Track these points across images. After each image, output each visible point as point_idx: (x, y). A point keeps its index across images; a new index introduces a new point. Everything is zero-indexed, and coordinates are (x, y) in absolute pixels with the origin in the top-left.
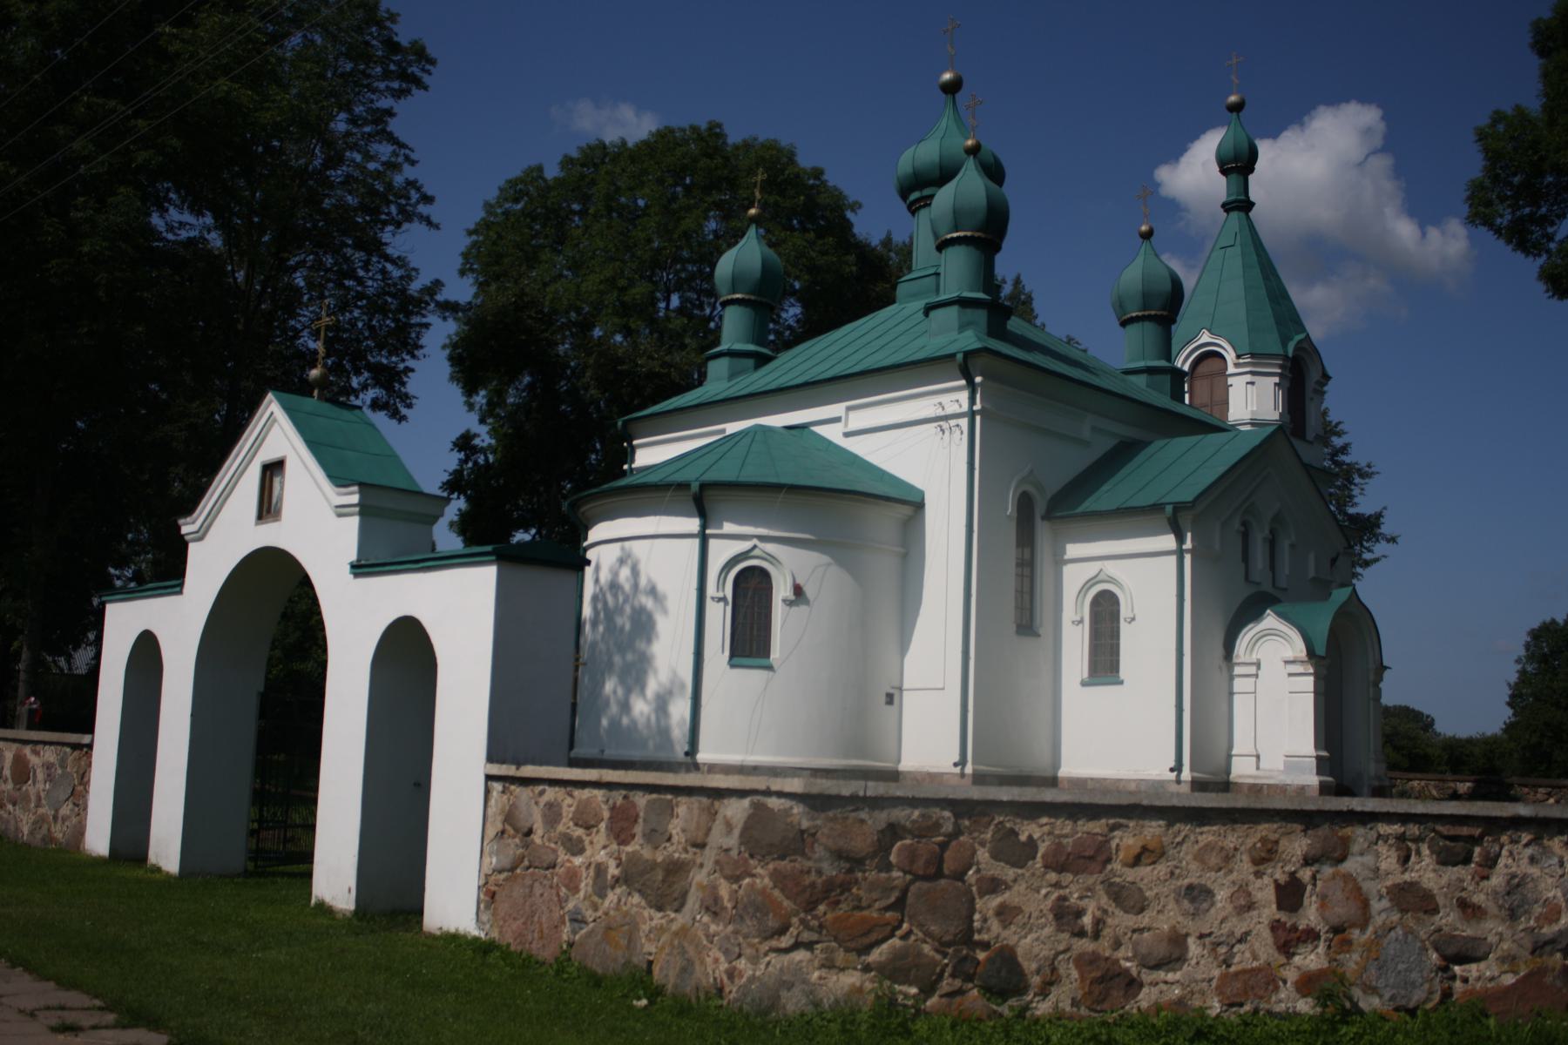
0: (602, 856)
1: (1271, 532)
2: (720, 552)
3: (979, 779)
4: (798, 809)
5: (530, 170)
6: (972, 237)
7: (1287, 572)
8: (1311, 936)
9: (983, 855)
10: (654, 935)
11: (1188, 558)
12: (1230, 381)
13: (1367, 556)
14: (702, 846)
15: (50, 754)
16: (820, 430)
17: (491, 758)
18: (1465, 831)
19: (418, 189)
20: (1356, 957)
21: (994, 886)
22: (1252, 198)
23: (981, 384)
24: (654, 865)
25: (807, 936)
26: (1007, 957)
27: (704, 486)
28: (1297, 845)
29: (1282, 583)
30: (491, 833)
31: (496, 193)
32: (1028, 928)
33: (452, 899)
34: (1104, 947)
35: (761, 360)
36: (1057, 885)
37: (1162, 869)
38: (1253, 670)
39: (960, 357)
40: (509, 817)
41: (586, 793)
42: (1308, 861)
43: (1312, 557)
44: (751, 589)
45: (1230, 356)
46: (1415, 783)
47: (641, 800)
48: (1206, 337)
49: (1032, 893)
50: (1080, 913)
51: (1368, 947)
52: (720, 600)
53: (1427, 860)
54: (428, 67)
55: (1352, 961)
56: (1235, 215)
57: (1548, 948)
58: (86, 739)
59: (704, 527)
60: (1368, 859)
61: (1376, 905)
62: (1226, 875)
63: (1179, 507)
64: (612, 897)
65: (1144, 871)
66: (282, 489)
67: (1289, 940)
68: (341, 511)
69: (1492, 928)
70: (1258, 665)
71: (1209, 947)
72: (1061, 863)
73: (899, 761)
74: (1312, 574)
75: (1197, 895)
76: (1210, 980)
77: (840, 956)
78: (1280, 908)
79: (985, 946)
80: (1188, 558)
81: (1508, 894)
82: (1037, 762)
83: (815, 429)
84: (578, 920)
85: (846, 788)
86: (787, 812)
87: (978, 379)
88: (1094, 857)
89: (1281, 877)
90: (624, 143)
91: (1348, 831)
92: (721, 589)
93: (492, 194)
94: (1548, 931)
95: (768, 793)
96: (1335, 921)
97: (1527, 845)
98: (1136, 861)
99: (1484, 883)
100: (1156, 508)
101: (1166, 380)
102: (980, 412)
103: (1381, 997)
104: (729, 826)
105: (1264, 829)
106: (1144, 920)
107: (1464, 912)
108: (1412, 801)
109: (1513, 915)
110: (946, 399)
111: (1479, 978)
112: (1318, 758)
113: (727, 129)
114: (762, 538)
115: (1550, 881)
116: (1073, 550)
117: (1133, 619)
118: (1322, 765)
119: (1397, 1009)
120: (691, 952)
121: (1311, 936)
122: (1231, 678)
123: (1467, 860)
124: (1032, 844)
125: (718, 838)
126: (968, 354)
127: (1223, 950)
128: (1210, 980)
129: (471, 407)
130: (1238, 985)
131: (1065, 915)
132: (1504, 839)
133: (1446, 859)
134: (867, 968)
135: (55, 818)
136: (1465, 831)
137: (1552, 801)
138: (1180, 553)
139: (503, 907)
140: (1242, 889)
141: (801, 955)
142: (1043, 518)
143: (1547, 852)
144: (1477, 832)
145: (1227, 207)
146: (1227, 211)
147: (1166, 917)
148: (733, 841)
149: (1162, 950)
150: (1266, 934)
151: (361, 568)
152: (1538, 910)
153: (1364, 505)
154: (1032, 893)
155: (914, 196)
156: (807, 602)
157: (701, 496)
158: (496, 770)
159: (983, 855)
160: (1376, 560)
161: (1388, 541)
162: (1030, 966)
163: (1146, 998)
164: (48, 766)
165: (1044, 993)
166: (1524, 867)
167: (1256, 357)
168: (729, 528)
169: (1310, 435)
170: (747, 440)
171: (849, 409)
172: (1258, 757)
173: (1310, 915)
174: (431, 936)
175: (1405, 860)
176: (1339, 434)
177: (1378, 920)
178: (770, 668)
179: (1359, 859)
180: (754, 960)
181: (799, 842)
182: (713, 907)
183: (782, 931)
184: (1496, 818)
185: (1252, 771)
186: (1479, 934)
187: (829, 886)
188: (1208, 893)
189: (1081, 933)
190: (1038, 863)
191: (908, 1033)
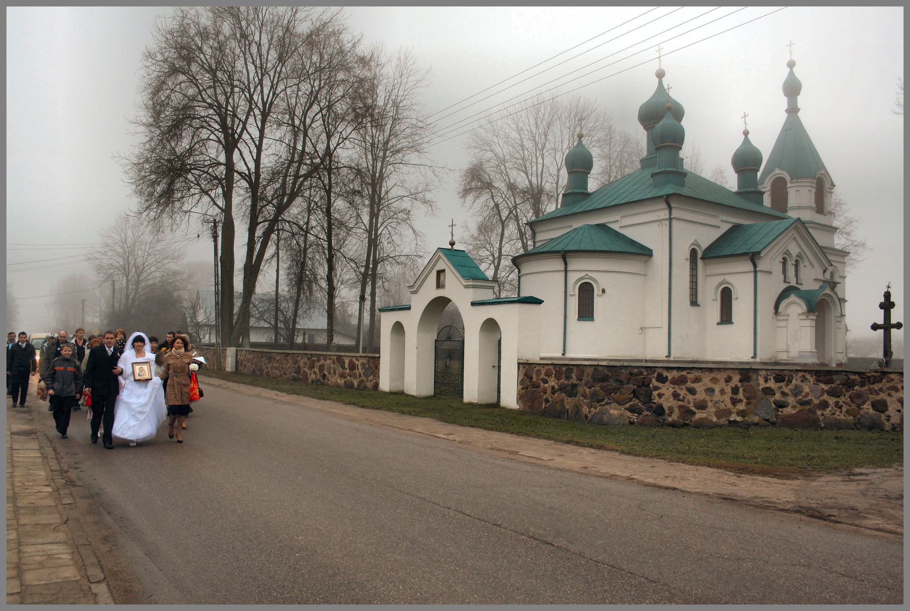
8: (741, 401)
9: (654, 380)
21: (656, 388)
24: (567, 385)
48: (777, 171)
49: (667, 390)
64: (556, 394)
67: (734, 402)
72: (675, 382)
75: (710, 391)
88: (682, 381)
92: (574, 291)
105: (729, 373)
109: (796, 396)
121: (741, 401)
123: (783, 381)
131: (676, 396)
147: (701, 395)
165: (670, 415)
170: (582, 232)
173: (741, 396)
174: (504, 408)
182: (584, 396)
187: (615, 389)
189: (679, 400)
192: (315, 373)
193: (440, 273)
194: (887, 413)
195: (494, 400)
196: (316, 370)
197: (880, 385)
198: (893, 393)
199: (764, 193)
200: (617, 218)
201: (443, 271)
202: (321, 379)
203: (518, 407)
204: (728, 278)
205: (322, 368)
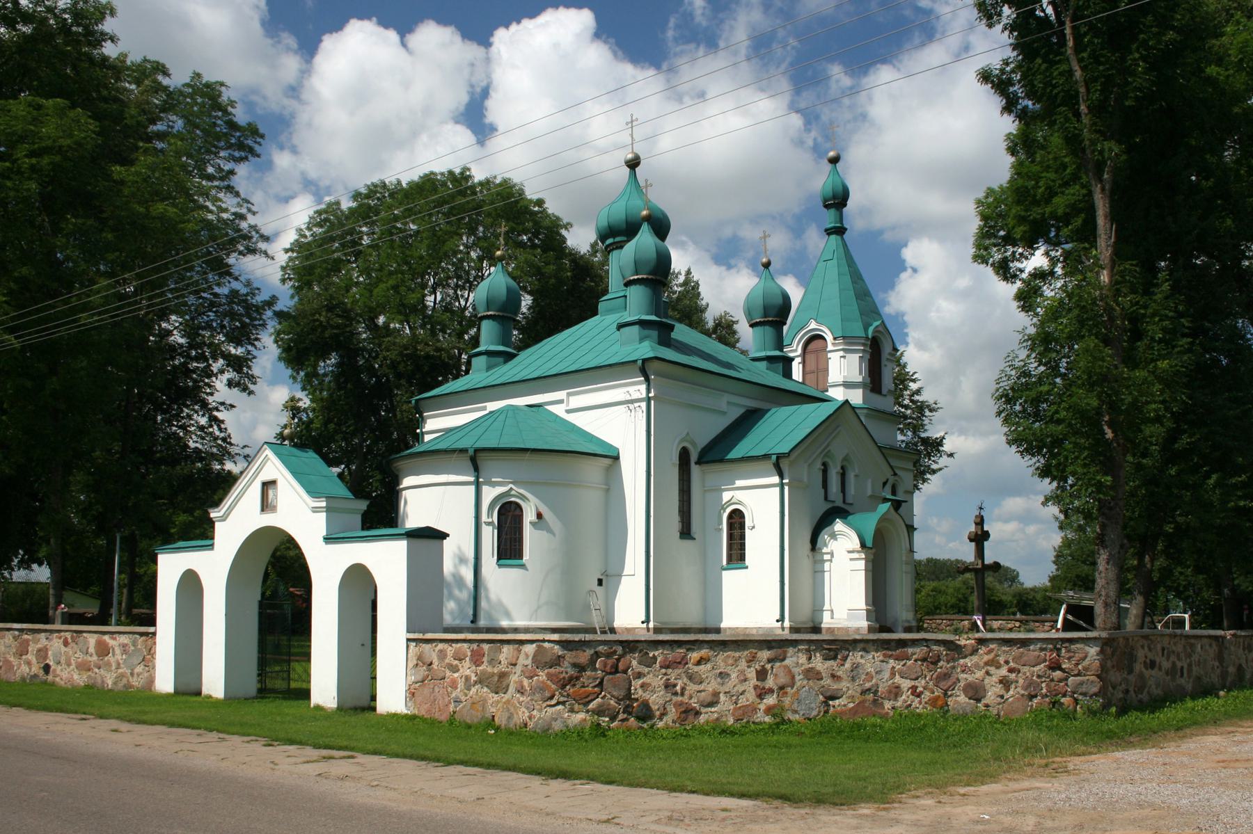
0: (468, 672)
1: (843, 468)
2: (489, 493)
3: (657, 630)
4: (557, 647)
8: (771, 691)
9: (634, 663)
10: (494, 704)
12: (829, 355)
13: (934, 466)
14: (515, 665)
15: (124, 639)
17: (408, 631)
19: (257, 232)
21: (639, 675)
24: (493, 675)
25: (562, 699)
26: (646, 705)
27: (477, 451)
28: (765, 654)
29: (849, 500)
30: (411, 665)
32: (654, 692)
33: (392, 696)
34: (685, 699)
35: (509, 357)
36: (665, 674)
37: (709, 666)
39: (640, 362)
40: (420, 658)
41: (459, 645)
42: (769, 661)
44: (509, 517)
47: (486, 647)
49: (655, 679)
50: (675, 686)
51: (794, 695)
54: (259, 140)
55: (787, 701)
56: (833, 237)
58: (151, 629)
59: (477, 478)
60: (794, 659)
61: (797, 678)
63: (780, 457)
64: (474, 690)
65: (702, 667)
66: (276, 496)
67: (762, 694)
68: (315, 510)
69: (844, 685)
72: (666, 666)
74: (869, 492)
77: (576, 706)
79: (637, 700)
80: (786, 488)
84: (457, 701)
85: (577, 637)
86: (552, 648)
88: (682, 662)
90: (399, 182)
92: (490, 518)
94: (868, 685)
95: (544, 641)
98: (699, 663)
100: (766, 457)
101: (780, 366)
102: (653, 398)
104: (527, 656)
106: (702, 687)
109: (853, 679)
110: (631, 389)
120: (512, 710)
121: (771, 691)
123: (835, 658)
124: (655, 658)
125: (522, 661)
131: (669, 686)
133: (826, 658)
134: (588, 711)
135: (132, 674)
138: (782, 486)
139: (419, 698)
140: (742, 672)
141: (560, 707)
147: (712, 685)
148: (529, 662)
149: (709, 699)
151: (328, 539)
152: (863, 677)
153: (933, 432)
154: (655, 679)
155: (609, 241)
157: (474, 459)
158: (412, 636)
159: (634, 663)
162: (655, 707)
163: (702, 719)
164: (124, 646)
167: (847, 339)
169: (884, 391)
170: (502, 417)
171: (569, 395)
173: (770, 682)
175: (810, 658)
176: (914, 381)
178: (523, 566)
180: (540, 711)
181: (558, 661)
182: (521, 691)
183: (552, 698)
188: (728, 675)
189: (676, 694)
190: (658, 665)
191: (605, 736)
192: (29, 663)
193: (268, 485)
194: (983, 701)
195: (365, 702)
196: (31, 657)
197: (975, 658)
198: (992, 670)
199: (792, 359)
200: (561, 395)
201: (274, 482)
202: (41, 672)
205: (43, 653)
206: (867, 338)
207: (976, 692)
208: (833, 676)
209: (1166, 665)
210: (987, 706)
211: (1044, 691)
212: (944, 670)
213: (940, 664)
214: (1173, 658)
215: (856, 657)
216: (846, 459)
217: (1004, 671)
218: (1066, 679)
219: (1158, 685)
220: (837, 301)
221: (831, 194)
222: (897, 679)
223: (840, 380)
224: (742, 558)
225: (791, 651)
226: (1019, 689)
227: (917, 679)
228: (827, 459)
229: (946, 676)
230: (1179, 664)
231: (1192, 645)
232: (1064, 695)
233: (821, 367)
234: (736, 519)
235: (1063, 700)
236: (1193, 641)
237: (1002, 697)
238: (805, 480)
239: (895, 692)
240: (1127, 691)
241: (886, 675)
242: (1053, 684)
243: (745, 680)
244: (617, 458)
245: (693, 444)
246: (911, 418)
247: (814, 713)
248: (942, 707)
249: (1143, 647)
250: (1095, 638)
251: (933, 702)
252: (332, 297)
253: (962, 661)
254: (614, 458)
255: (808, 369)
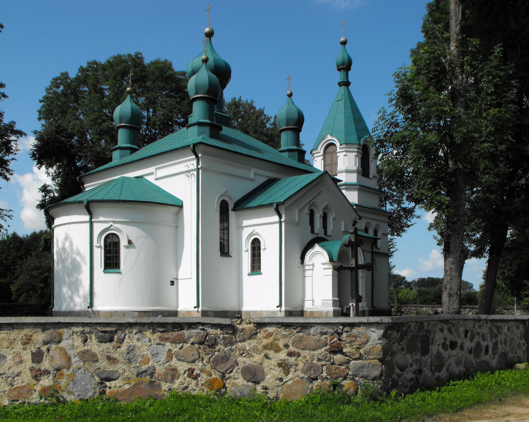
2: (98, 228)
5: (62, 74)
6: (203, 97)
7: (331, 229)
11: (283, 224)
12: (338, 155)
13: (409, 223)
16: (147, 178)
18: (108, 329)
20: (65, 380)
22: (350, 81)
23: (201, 156)
29: (329, 233)
31: (50, 83)
35: (133, 151)
38: (311, 267)
39: (192, 146)
42: (45, 343)
43: (343, 223)
45: (338, 144)
46: (424, 308)
48: (329, 137)
51: (69, 376)
52: (99, 247)
53: (94, 341)
55: (63, 382)
56: (343, 87)
57: (144, 374)
59: (91, 218)
60: (70, 342)
61: (74, 360)
62: (11, 350)
67: (37, 375)
69: (120, 367)
70: (313, 265)
71: (4, 378)
73: (178, 307)
74: (343, 229)
76: (4, 392)
78: (33, 362)
80: (283, 224)
81: (128, 353)
82: (230, 305)
83: (146, 177)
87: (200, 155)
89: (34, 350)
91: (61, 330)
93: (48, 84)
94: (144, 368)
96: (56, 366)
97: (136, 334)
99: (119, 349)
100: (271, 205)
103: (74, 395)
107: (110, 361)
108: (85, 318)
109: (130, 361)
111: (115, 387)
112: (333, 300)
113: (144, 55)
114: (113, 222)
115: (145, 347)
116: (246, 223)
117: (265, 249)
118: (334, 303)
119: (80, 400)
122: (304, 271)
123: (111, 340)
126: (195, 145)
127: (10, 379)
128: (4, 392)
129: (48, 174)
130: (16, 393)
132: (127, 332)
133: (102, 341)
136: (108, 329)
137: (470, 313)
138: (280, 223)
142: (232, 210)
143: (144, 336)
144: (114, 329)
145: (340, 84)
146: (340, 86)
150: (28, 373)
156: (135, 247)
160: (412, 225)
161: (417, 217)
166: (135, 343)
167: (347, 144)
168: (101, 219)
169: (371, 176)
171: (157, 169)
172: (313, 301)
173: (46, 364)
175: (85, 341)
177: (75, 365)
178: (120, 273)
179: (66, 341)
184: (122, 323)
185: (311, 306)
186: (115, 369)
194: (262, 384)
198: (271, 353)
203: (383, 331)
204: (257, 229)
206: (360, 145)
207: (254, 375)
208: (109, 358)
209: (468, 344)
210: (265, 388)
211: (324, 374)
212: (222, 354)
213: (217, 348)
214: (476, 339)
215: (131, 339)
216: (326, 208)
217: (283, 355)
218: (348, 362)
219: (458, 364)
220: (343, 125)
221: (341, 62)
222: (174, 362)
223: (344, 168)
224: (259, 268)
225: (66, 332)
226: (299, 373)
227: (193, 362)
228: (325, 211)
229: (225, 358)
230: (484, 344)
231: (498, 328)
232: (345, 378)
233: (333, 162)
234: (256, 245)
235: (344, 383)
236: (499, 324)
237: (281, 380)
238: (297, 219)
239: (173, 374)
240: (420, 371)
241: (163, 357)
242: (334, 367)
243: (21, 362)
244: (181, 207)
245: (231, 198)
246: (396, 196)
247: (90, 394)
248: (219, 390)
249: (442, 330)
250: (377, 323)
251: (210, 384)
252: (59, 126)
253: (240, 345)
254: (180, 207)
255: (327, 163)
